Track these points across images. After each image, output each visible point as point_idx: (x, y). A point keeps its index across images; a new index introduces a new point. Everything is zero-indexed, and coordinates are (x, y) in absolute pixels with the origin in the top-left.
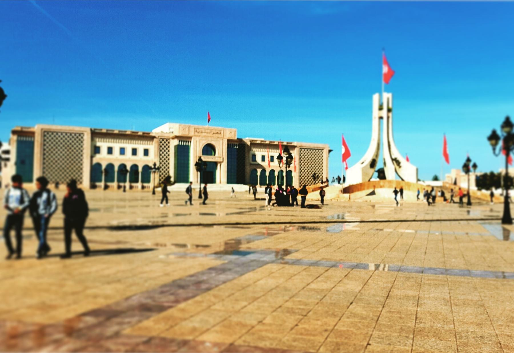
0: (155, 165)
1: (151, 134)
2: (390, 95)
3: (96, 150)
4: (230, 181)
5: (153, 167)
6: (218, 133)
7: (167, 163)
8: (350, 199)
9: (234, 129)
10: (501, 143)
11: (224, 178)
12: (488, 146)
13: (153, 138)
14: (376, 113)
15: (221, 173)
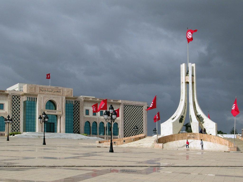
0: (9, 117)
1: (6, 92)
2: (194, 65)
4: (68, 131)
5: (7, 119)
6: (58, 92)
7: (18, 115)
8: (163, 147)
9: (71, 89)
11: (63, 129)
13: (7, 95)
14: (183, 79)
15: (61, 125)
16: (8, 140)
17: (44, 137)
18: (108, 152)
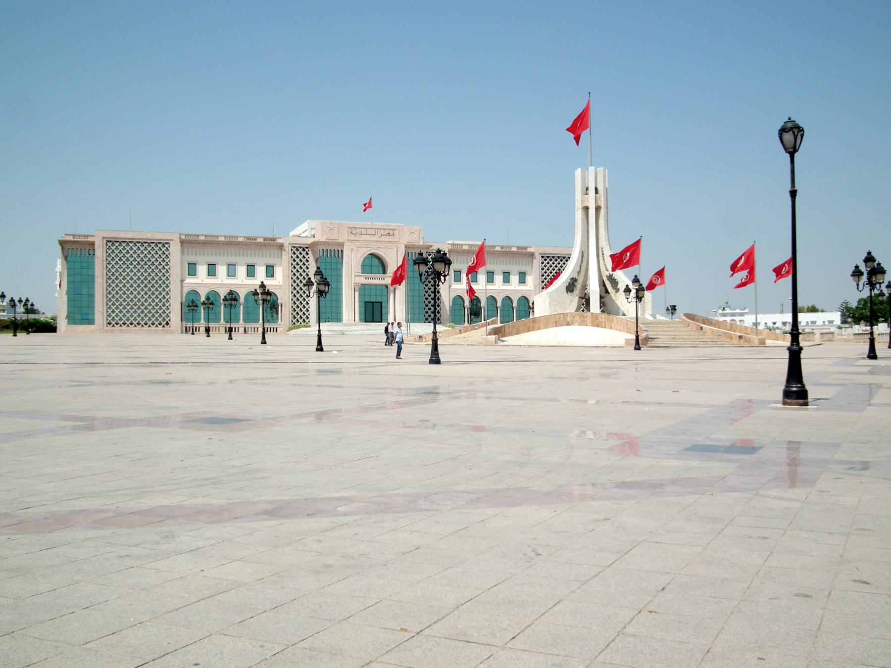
3: (192, 269)
10: (864, 278)
12: (852, 282)
16: (264, 342)
17: (319, 331)
18: (423, 363)
